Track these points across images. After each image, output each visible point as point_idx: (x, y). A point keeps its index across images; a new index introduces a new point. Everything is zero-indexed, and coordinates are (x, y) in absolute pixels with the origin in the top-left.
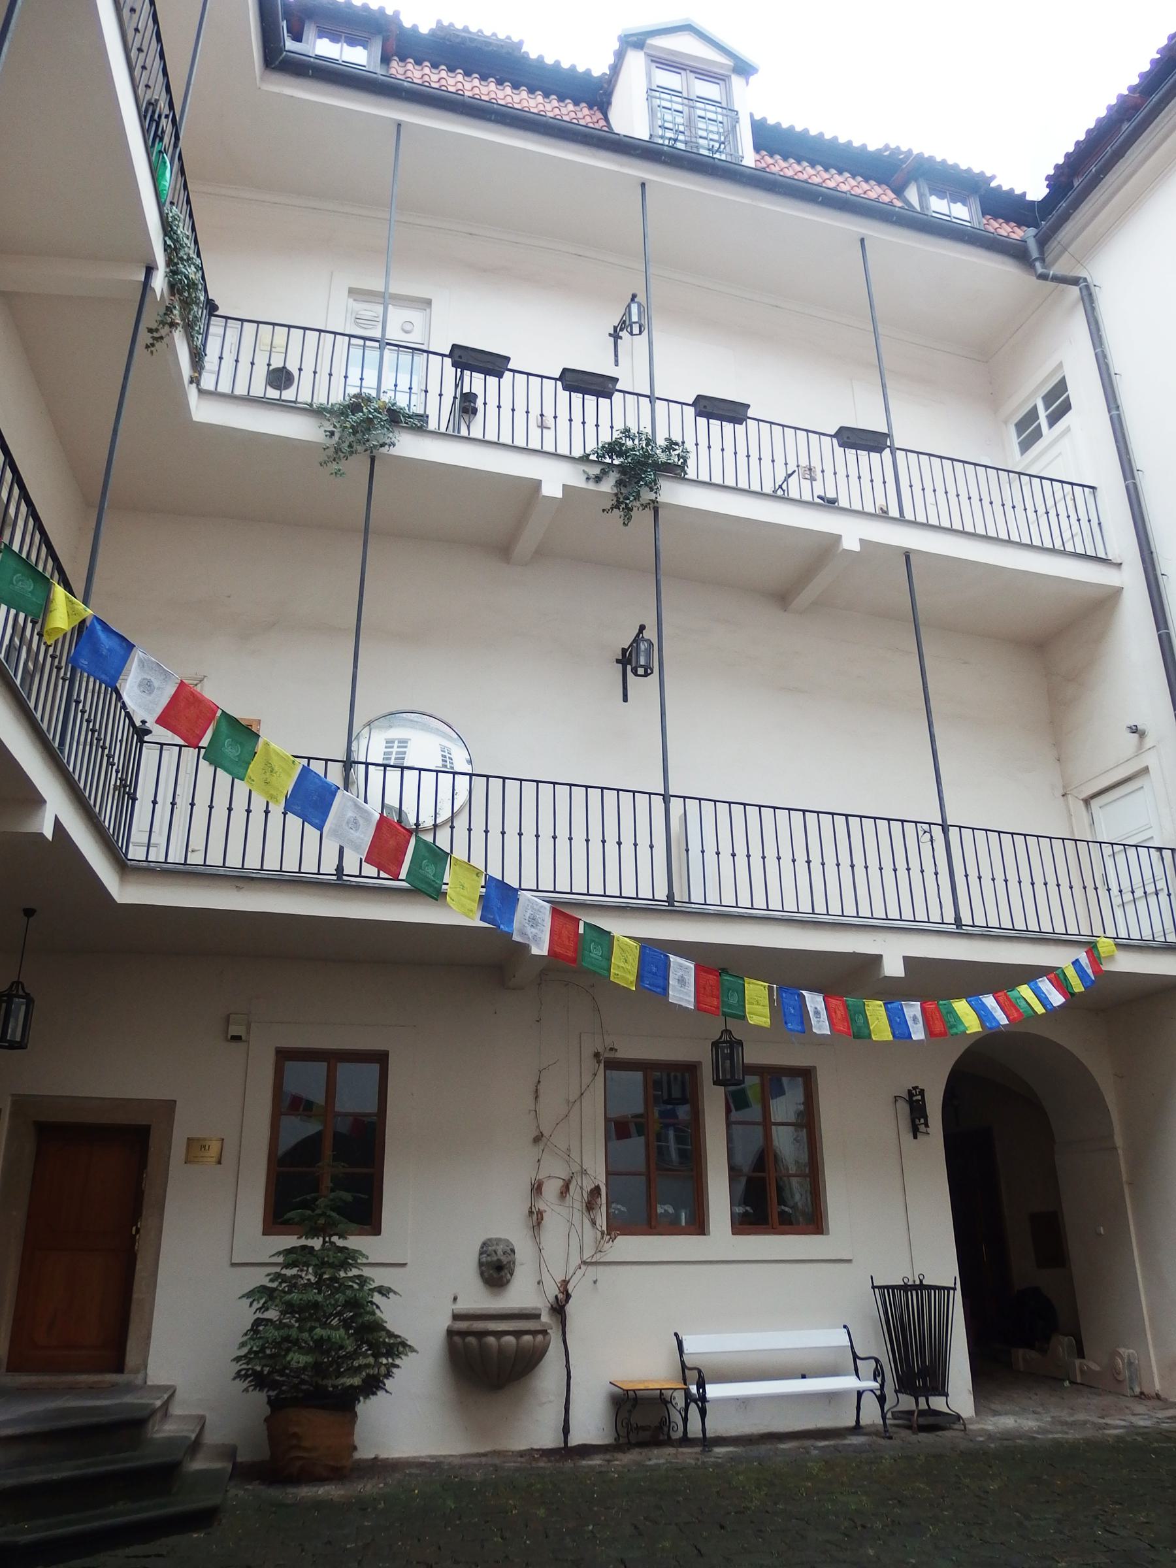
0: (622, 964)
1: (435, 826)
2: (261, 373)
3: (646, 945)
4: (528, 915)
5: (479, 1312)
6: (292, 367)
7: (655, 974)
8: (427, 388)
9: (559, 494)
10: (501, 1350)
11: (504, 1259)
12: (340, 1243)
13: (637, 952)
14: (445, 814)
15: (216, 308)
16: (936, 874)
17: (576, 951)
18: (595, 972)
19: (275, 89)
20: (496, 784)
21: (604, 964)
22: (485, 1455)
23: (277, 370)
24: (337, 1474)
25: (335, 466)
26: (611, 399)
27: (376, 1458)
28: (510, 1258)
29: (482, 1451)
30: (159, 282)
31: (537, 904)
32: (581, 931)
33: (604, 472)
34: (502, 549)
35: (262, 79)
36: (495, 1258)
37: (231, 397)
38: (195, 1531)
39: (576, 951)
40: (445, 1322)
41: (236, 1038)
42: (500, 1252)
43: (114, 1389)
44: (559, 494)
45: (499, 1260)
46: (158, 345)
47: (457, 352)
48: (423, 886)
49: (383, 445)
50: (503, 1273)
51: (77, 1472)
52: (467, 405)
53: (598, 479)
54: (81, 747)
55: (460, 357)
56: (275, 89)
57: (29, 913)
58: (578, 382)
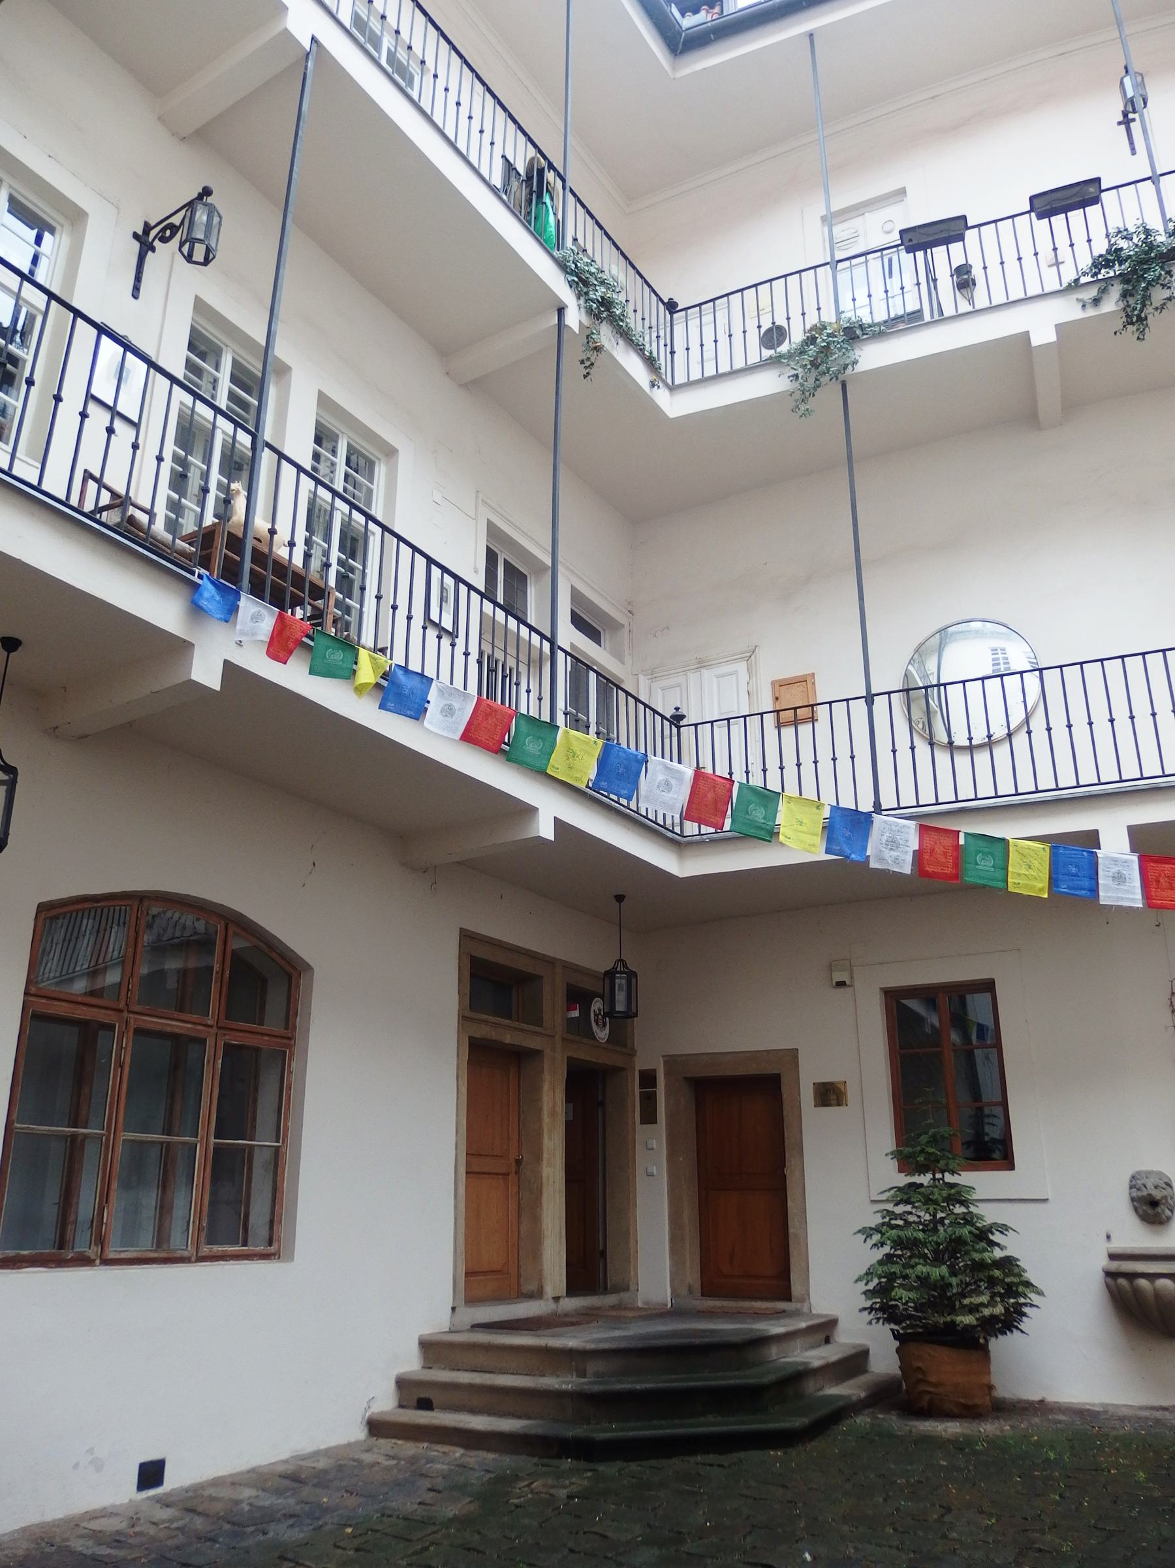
0: (1023, 871)
1: (1009, 735)
2: (754, 338)
3: (1055, 842)
4: (885, 838)
5: (1129, 1252)
6: (781, 321)
7: (1076, 875)
8: (865, 296)
9: (1052, 337)
10: (1157, 1295)
11: (1157, 1194)
12: (949, 1178)
13: (1046, 855)
14: (1017, 717)
15: (676, 305)
16: (799, 765)
17: (956, 865)
18: (984, 886)
19: (687, 71)
20: (1072, 674)
21: (999, 874)
22: (1152, 1408)
23: (770, 330)
24: (970, 1412)
25: (803, 407)
26: (963, 240)
27: (1042, 1402)
28: (1165, 1193)
29: (1165, 1404)
30: (575, 317)
31: (897, 824)
32: (962, 841)
33: (1103, 291)
34: (1028, 417)
35: (674, 69)
36: (1145, 1193)
37: (704, 381)
38: (772, 1449)
39: (956, 865)
40: (1103, 1262)
41: (841, 984)
42: (1150, 1185)
43: (781, 1314)
44: (1052, 337)
45: (1150, 1195)
46: (592, 371)
47: (906, 237)
48: (752, 832)
49: (845, 367)
50: (1159, 1210)
51: (660, 1385)
52: (964, 279)
53: (1096, 301)
54: (667, 741)
55: (910, 240)
56: (687, 71)
57: (620, 898)
58: (1051, 204)
